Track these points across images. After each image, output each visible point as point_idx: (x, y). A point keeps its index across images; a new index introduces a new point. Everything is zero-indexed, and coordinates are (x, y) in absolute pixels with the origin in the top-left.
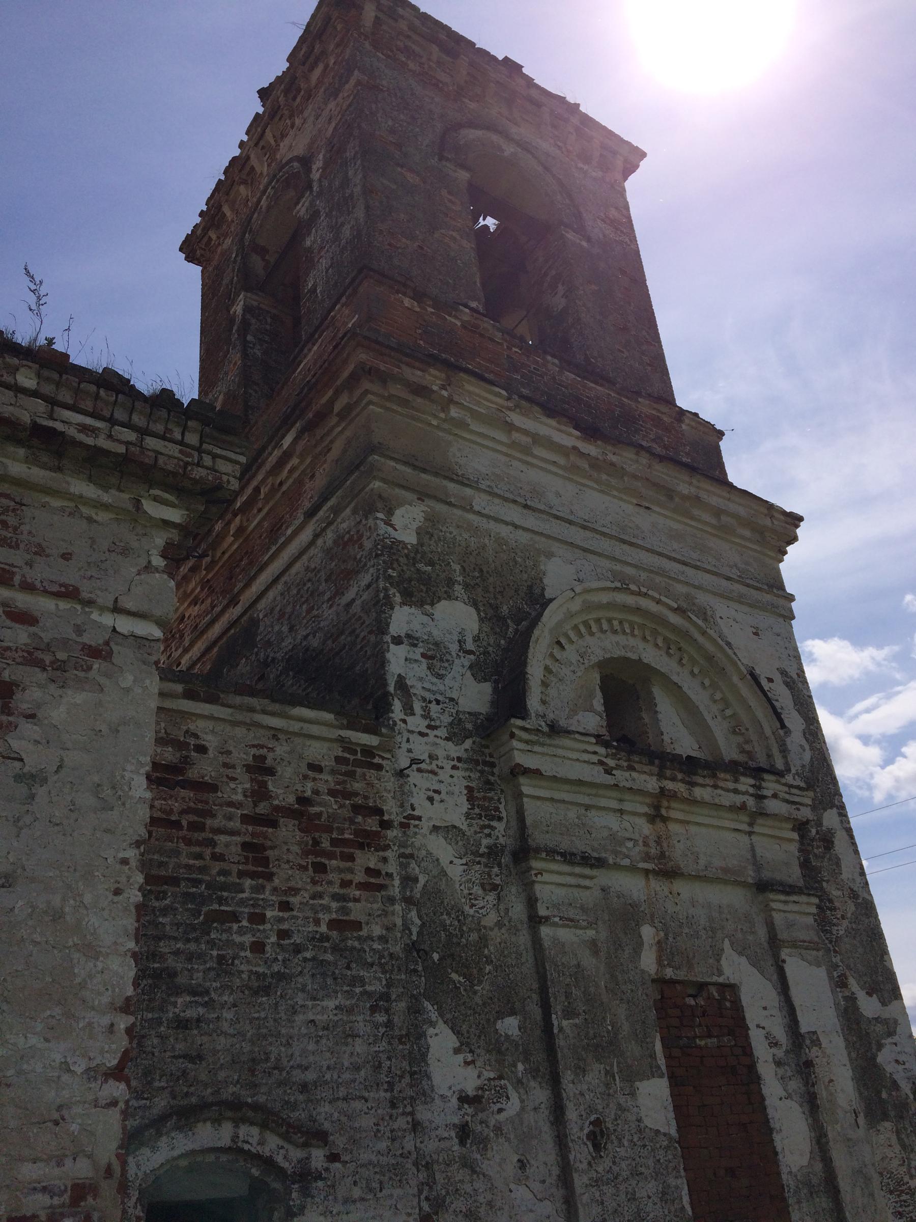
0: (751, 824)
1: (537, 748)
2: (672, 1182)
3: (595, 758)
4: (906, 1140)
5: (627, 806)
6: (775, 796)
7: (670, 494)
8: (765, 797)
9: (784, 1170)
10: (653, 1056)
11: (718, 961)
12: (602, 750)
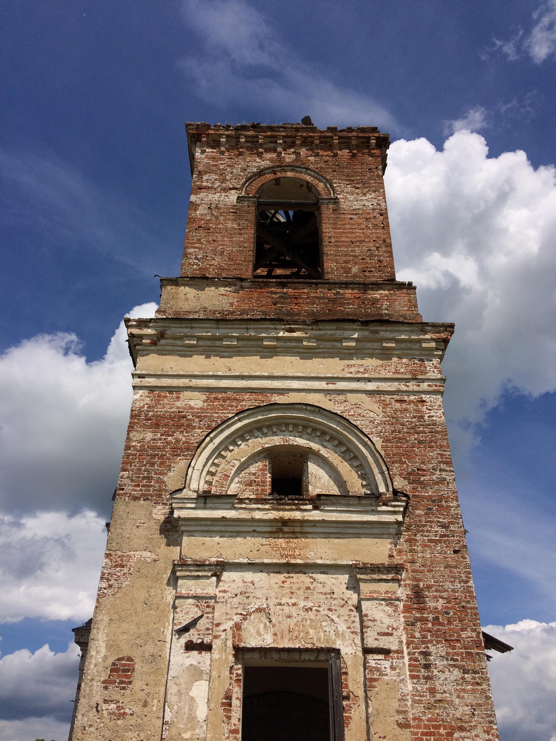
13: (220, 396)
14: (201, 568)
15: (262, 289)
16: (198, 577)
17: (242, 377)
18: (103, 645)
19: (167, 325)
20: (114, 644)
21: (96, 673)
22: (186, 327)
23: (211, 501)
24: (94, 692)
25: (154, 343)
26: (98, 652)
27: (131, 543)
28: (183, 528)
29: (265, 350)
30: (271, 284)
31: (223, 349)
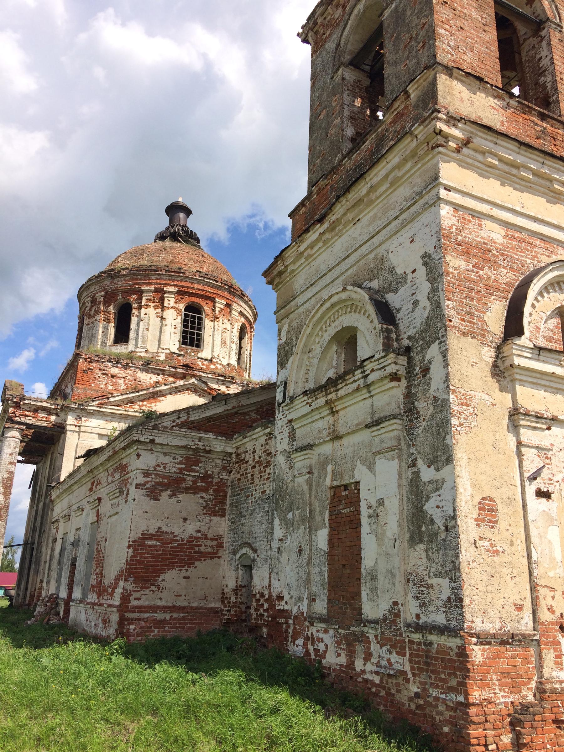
0: (370, 392)
1: (291, 410)
2: (323, 568)
3: (305, 403)
4: (431, 555)
5: (322, 415)
6: (373, 370)
7: (360, 201)
8: (368, 375)
9: (363, 567)
10: (324, 520)
11: (353, 472)
12: (306, 398)
13: (516, 235)
14: (540, 420)
15: (525, 114)
16: (536, 428)
17: (535, 219)
18: (468, 483)
19: (475, 131)
20: (476, 483)
21: (468, 511)
22: (491, 141)
23: (544, 355)
24: (470, 528)
25: (458, 151)
26: (465, 490)
27: (470, 382)
28: (518, 377)
29: (552, 194)
30: (534, 112)
31: (517, 180)
